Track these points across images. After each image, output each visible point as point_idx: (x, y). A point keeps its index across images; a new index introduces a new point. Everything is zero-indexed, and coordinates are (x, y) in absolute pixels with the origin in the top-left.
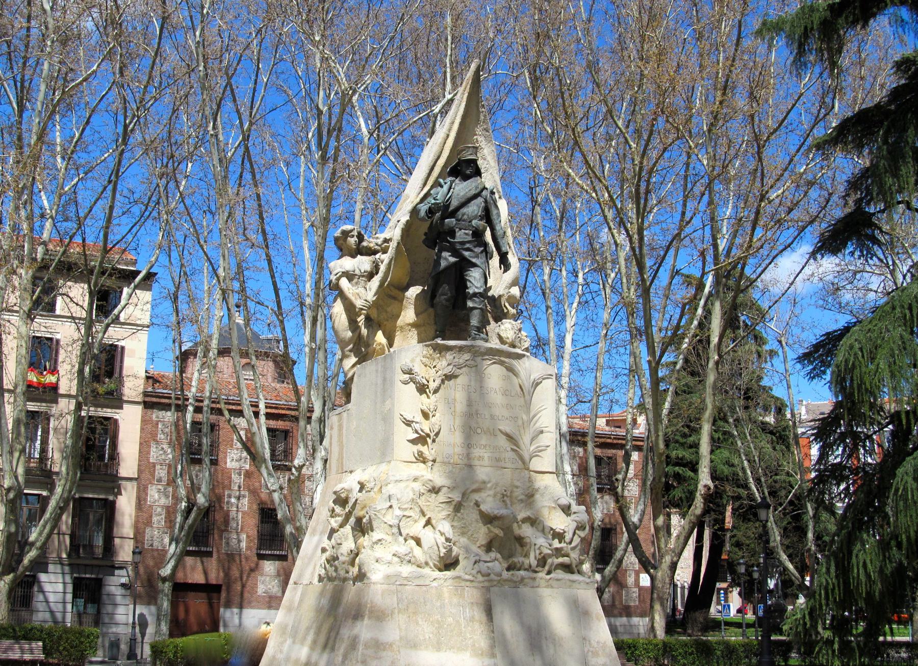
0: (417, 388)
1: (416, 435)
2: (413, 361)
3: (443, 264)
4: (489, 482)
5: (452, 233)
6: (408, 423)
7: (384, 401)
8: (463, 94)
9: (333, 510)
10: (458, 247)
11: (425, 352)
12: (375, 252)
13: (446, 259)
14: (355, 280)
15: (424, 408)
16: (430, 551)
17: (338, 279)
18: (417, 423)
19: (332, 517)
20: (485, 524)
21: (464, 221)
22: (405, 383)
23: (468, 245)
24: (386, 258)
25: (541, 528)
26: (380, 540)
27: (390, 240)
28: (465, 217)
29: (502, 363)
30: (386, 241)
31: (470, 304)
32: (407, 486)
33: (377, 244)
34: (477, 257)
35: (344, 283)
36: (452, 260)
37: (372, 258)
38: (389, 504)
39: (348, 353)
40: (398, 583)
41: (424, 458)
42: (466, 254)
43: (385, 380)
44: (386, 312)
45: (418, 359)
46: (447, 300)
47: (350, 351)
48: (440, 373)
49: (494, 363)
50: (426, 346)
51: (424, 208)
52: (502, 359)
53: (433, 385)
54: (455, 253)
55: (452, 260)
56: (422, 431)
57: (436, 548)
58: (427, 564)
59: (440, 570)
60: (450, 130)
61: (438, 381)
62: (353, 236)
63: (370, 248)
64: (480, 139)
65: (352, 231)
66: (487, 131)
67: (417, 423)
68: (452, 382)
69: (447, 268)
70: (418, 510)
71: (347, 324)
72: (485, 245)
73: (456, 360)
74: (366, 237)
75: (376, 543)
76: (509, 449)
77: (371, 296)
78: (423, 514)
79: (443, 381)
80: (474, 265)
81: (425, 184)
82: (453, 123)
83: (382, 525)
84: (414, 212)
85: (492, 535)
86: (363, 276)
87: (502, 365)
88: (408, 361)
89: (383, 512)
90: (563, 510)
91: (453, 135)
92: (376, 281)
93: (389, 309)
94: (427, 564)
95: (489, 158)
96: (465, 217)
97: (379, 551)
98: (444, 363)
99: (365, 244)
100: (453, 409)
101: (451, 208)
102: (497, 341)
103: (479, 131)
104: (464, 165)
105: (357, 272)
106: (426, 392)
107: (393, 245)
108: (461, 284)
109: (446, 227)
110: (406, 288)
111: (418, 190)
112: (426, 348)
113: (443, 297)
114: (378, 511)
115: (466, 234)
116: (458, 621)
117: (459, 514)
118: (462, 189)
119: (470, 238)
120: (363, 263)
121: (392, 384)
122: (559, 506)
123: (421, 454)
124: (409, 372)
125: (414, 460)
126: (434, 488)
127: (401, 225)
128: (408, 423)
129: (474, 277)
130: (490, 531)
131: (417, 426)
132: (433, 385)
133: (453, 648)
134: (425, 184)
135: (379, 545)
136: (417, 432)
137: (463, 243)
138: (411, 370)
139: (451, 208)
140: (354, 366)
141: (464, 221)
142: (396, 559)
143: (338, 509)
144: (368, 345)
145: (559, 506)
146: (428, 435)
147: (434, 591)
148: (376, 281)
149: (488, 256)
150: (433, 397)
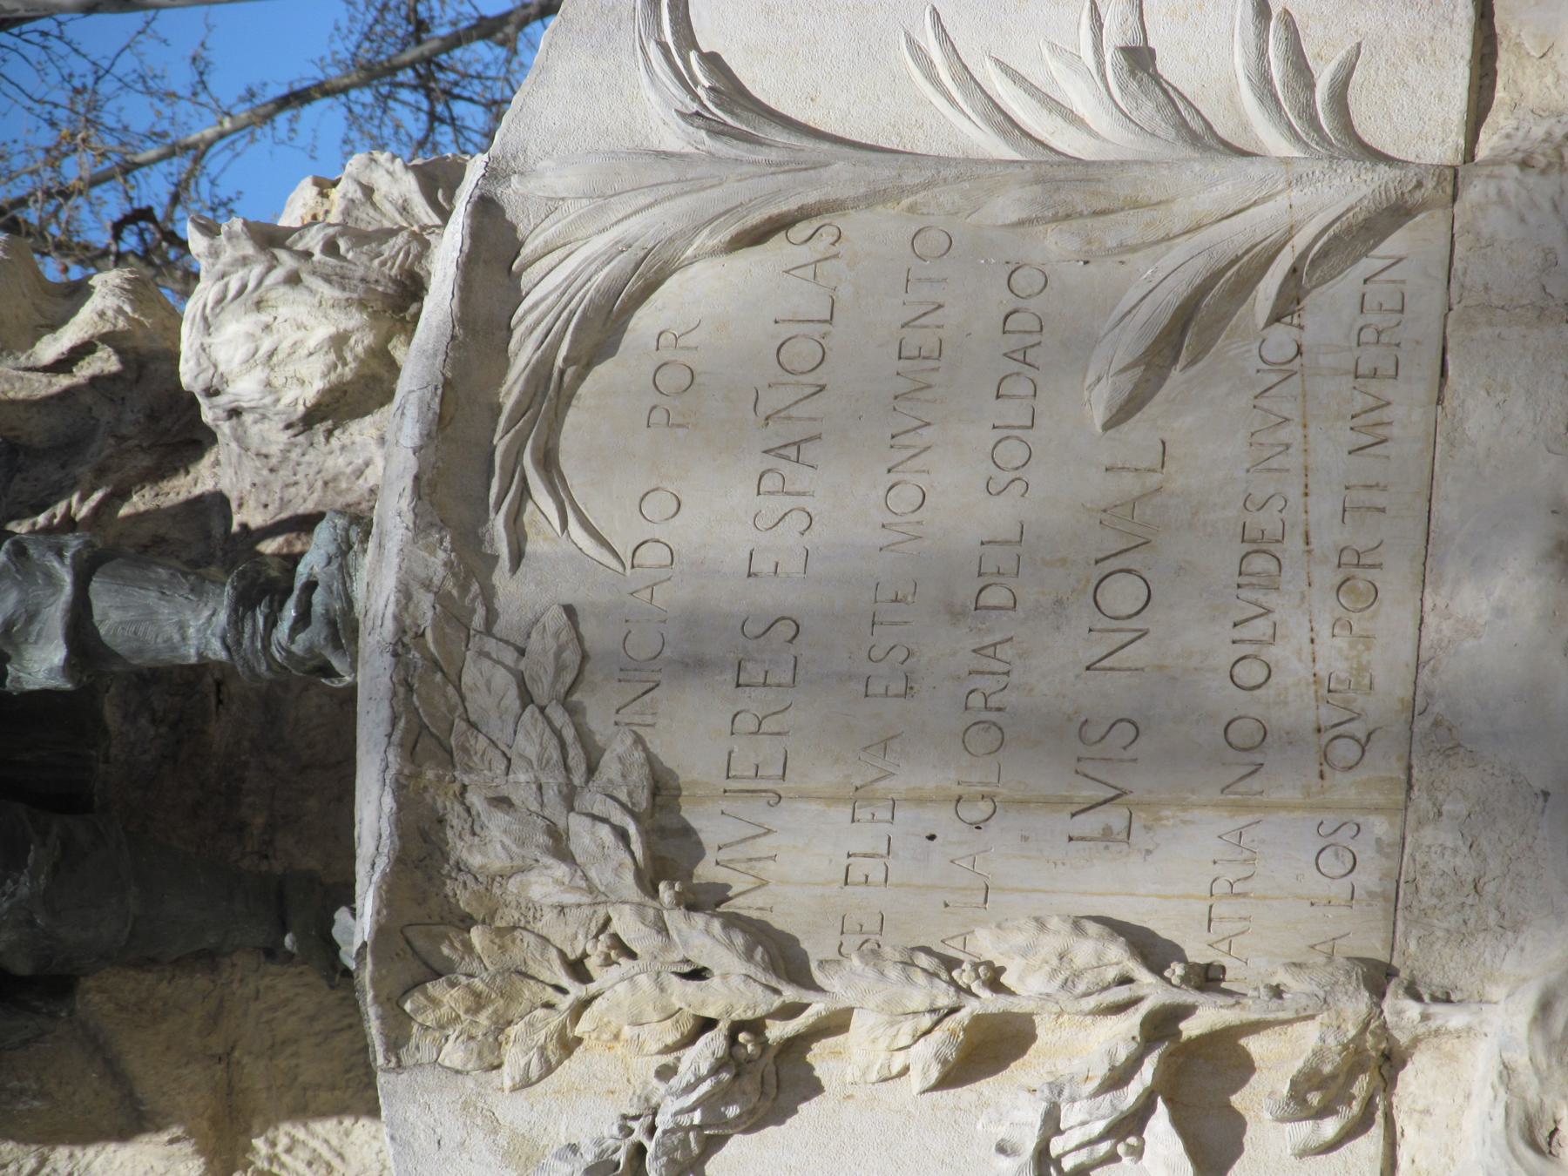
0: (753, 1122)
11: (454, 1054)
18: (1052, 1124)
41: (1355, 1061)
45: (514, 1111)
56: (1118, 1078)
67: (1052, 1124)
79: (703, 900)
87: (565, 398)
98: (545, 885)
102: (362, 431)
123: (1314, 1092)
125: (1369, 1145)
132: (736, 989)
146: (1161, 1025)
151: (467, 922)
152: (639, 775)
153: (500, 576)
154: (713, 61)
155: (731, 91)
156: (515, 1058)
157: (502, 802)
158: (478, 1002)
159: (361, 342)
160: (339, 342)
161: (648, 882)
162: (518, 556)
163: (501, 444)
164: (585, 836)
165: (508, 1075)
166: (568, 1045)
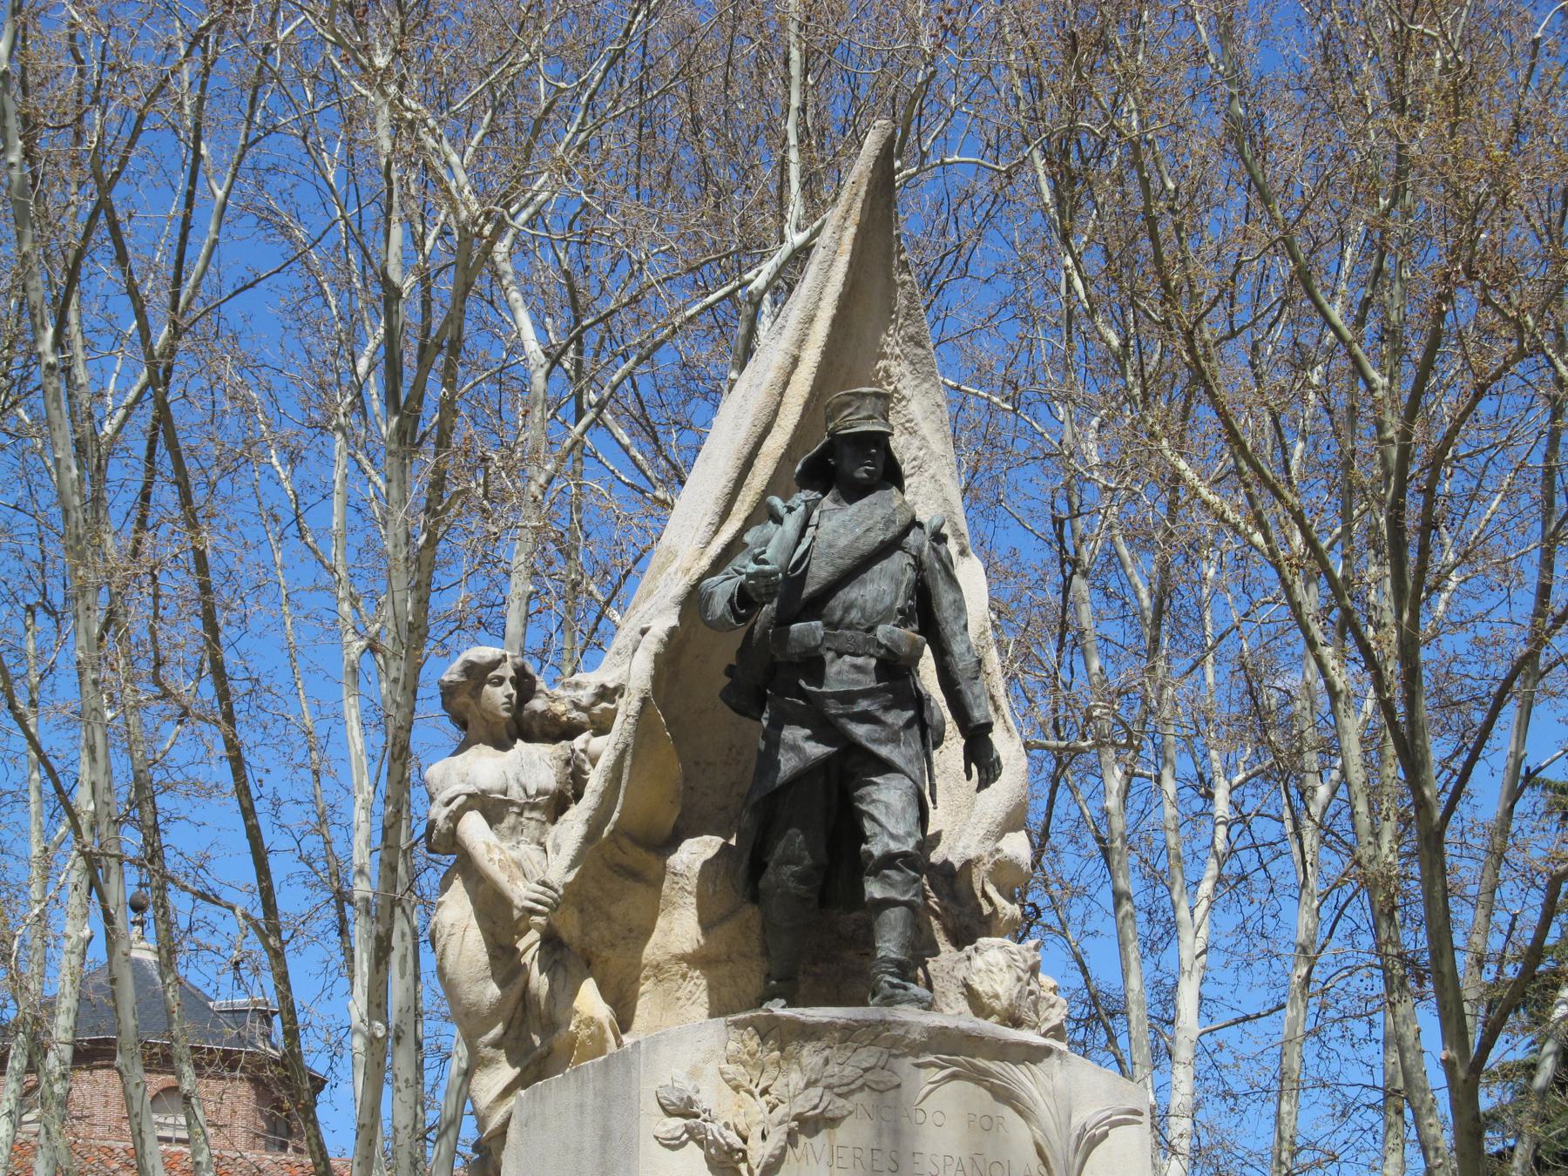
0: (709, 1159)
2: (694, 1073)
3: (788, 764)
5: (813, 666)
8: (842, 228)
10: (834, 709)
11: (732, 1046)
12: (569, 731)
13: (795, 748)
14: (510, 820)
17: (455, 817)
21: (850, 627)
22: (673, 1145)
23: (863, 705)
24: (605, 748)
27: (619, 690)
28: (854, 615)
29: (979, 1077)
33: (576, 706)
34: (894, 739)
35: (474, 828)
36: (816, 750)
37: (561, 749)
39: (488, 1052)
42: (860, 731)
43: (606, 1135)
44: (609, 918)
45: (711, 1069)
46: (802, 879)
47: (496, 1044)
48: (781, 1110)
49: (954, 1076)
51: (723, 589)
52: (980, 1062)
54: (824, 729)
55: (816, 750)
60: (801, 342)
61: (777, 1138)
62: (500, 681)
64: (895, 370)
65: (495, 664)
66: (919, 344)
69: (799, 777)
72: (919, 702)
74: (541, 685)
77: (558, 868)
79: (792, 1138)
80: (886, 767)
81: (725, 515)
82: (810, 320)
84: (694, 601)
86: (534, 807)
87: (978, 1082)
91: (811, 357)
92: (575, 821)
93: (616, 910)
95: (926, 428)
96: (854, 615)
98: (796, 1079)
99: (538, 704)
101: (810, 588)
102: (963, 1006)
103: (892, 341)
105: (515, 794)
107: (627, 706)
108: (844, 827)
109: (794, 649)
110: (672, 843)
111: (703, 531)
112: (735, 1034)
118: (842, 526)
119: (869, 682)
120: (532, 766)
127: (651, 645)
129: (886, 803)
134: (725, 515)
137: (848, 698)
138: (690, 1102)
141: (850, 627)
148: (575, 821)
149: (930, 736)
151: (782, 1050)
152: (838, 1113)
154: (1105, 1135)
155: (1094, 1142)
156: (731, 1069)
157: (827, 1062)
158: (752, 1055)
159: (997, 1005)
160: (996, 996)
161: (798, 1117)
162: (919, 1066)
163: (960, 1059)
164: (815, 1092)
165: (724, 1066)
166: (736, 1089)
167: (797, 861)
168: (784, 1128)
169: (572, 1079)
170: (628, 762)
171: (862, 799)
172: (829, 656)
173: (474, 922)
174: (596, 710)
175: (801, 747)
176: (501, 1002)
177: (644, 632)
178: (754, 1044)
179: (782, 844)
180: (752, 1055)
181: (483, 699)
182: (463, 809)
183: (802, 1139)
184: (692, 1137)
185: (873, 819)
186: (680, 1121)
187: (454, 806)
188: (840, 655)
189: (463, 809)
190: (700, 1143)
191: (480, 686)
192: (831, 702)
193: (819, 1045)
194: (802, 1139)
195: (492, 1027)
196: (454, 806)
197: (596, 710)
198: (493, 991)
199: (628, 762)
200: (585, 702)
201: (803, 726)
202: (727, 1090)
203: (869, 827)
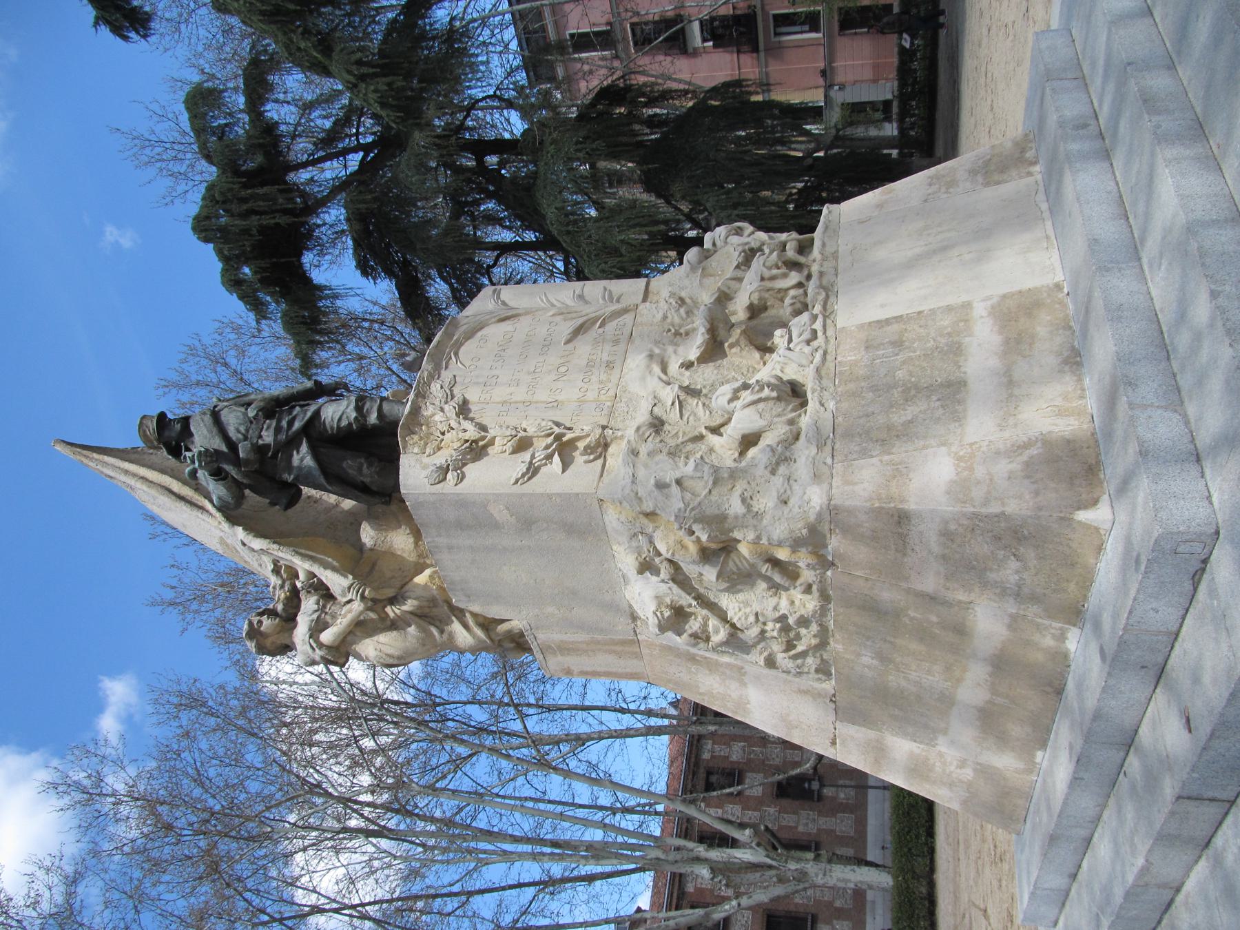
0: (474, 460)
1: (556, 457)
4: (651, 350)
5: (261, 450)
6: (532, 471)
7: (496, 526)
9: (695, 636)
10: (282, 437)
13: (302, 460)
14: (328, 618)
15: (509, 447)
16: (768, 416)
17: (321, 645)
19: (708, 639)
20: (724, 355)
21: (247, 431)
23: (284, 423)
24: (302, 566)
25: (733, 284)
26: (743, 501)
27: (276, 563)
29: (459, 345)
30: (276, 571)
31: (373, 418)
32: (646, 466)
33: (282, 587)
35: (327, 636)
36: (304, 448)
37: (302, 595)
38: (675, 489)
39: (445, 636)
40: (829, 461)
42: (297, 425)
43: (460, 525)
45: (426, 460)
46: (370, 465)
47: (442, 632)
48: (453, 424)
49: (456, 354)
50: (404, 448)
53: (472, 433)
54: (292, 443)
55: (304, 448)
56: (547, 447)
57: (761, 406)
58: (791, 422)
59: (804, 404)
60: (134, 475)
61: (467, 425)
62: (260, 622)
63: (287, 598)
65: (251, 624)
68: (473, 407)
70: (690, 446)
71: (395, 633)
73: (437, 402)
75: (749, 507)
76: (601, 330)
78: (700, 438)
81: (202, 508)
83: (713, 498)
85: (743, 342)
86: (324, 606)
87: (462, 345)
88: (425, 473)
89: (688, 496)
90: (707, 258)
94: (791, 422)
96: (242, 429)
97: (766, 502)
99: (280, 607)
100: (520, 405)
101: (225, 449)
104: (167, 433)
105: (315, 616)
106: (485, 447)
107: (287, 556)
109: (252, 456)
110: (360, 547)
111: (210, 520)
112: (410, 449)
113: (365, 470)
114: (687, 505)
115: (268, 428)
116: (904, 363)
117: (704, 391)
121: (462, 503)
122: (700, 262)
123: (588, 450)
124: (444, 471)
125: (600, 461)
126: (652, 425)
128: (532, 471)
130: (736, 344)
131: (540, 455)
133: (956, 363)
134: (202, 508)
135: (754, 503)
136: (549, 457)
137: (278, 430)
138: (440, 468)
139: (225, 449)
140: (466, 626)
142: (782, 469)
143: (694, 625)
144: (433, 601)
145: (700, 262)
147: (845, 405)
150: (492, 433)
153: (443, 372)
158: (421, 439)
161: (458, 415)
166: (439, 449)
167: (362, 465)
168: (462, 421)
169: (437, 557)
170: (303, 551)
171: (332, 428)
172: (260, 442)
173: (376, 638)
174: (285, 576)
175: (303, 457)
176: (418, 626)
177: (244, 544)
178: (416, 437)
179: (350, 471)
180: (421, 439)
181: (268, 631)
182: (317, 641)
183: (471, 415)
184: (460, 469)
185: (340, 419)
186: (449, 476)
187: (314, 645)
188: (260, 437)
189: (317, 641)
190: (464, 465)
191: (261, 634)
192: (279, 437)
193: (424, 407)
194: (471, 415)
195: (432, 634)
196: (314, 645)
197: (285, 576)
198: (412, 630)
199: (303, 551)
200: (280, 582)
201: (292, 456)
202: (439, 453)
203: (344, 423)
